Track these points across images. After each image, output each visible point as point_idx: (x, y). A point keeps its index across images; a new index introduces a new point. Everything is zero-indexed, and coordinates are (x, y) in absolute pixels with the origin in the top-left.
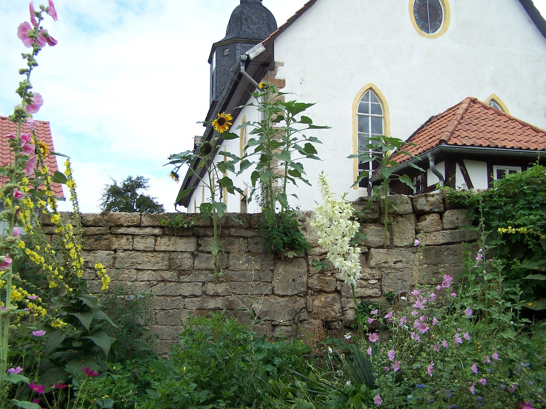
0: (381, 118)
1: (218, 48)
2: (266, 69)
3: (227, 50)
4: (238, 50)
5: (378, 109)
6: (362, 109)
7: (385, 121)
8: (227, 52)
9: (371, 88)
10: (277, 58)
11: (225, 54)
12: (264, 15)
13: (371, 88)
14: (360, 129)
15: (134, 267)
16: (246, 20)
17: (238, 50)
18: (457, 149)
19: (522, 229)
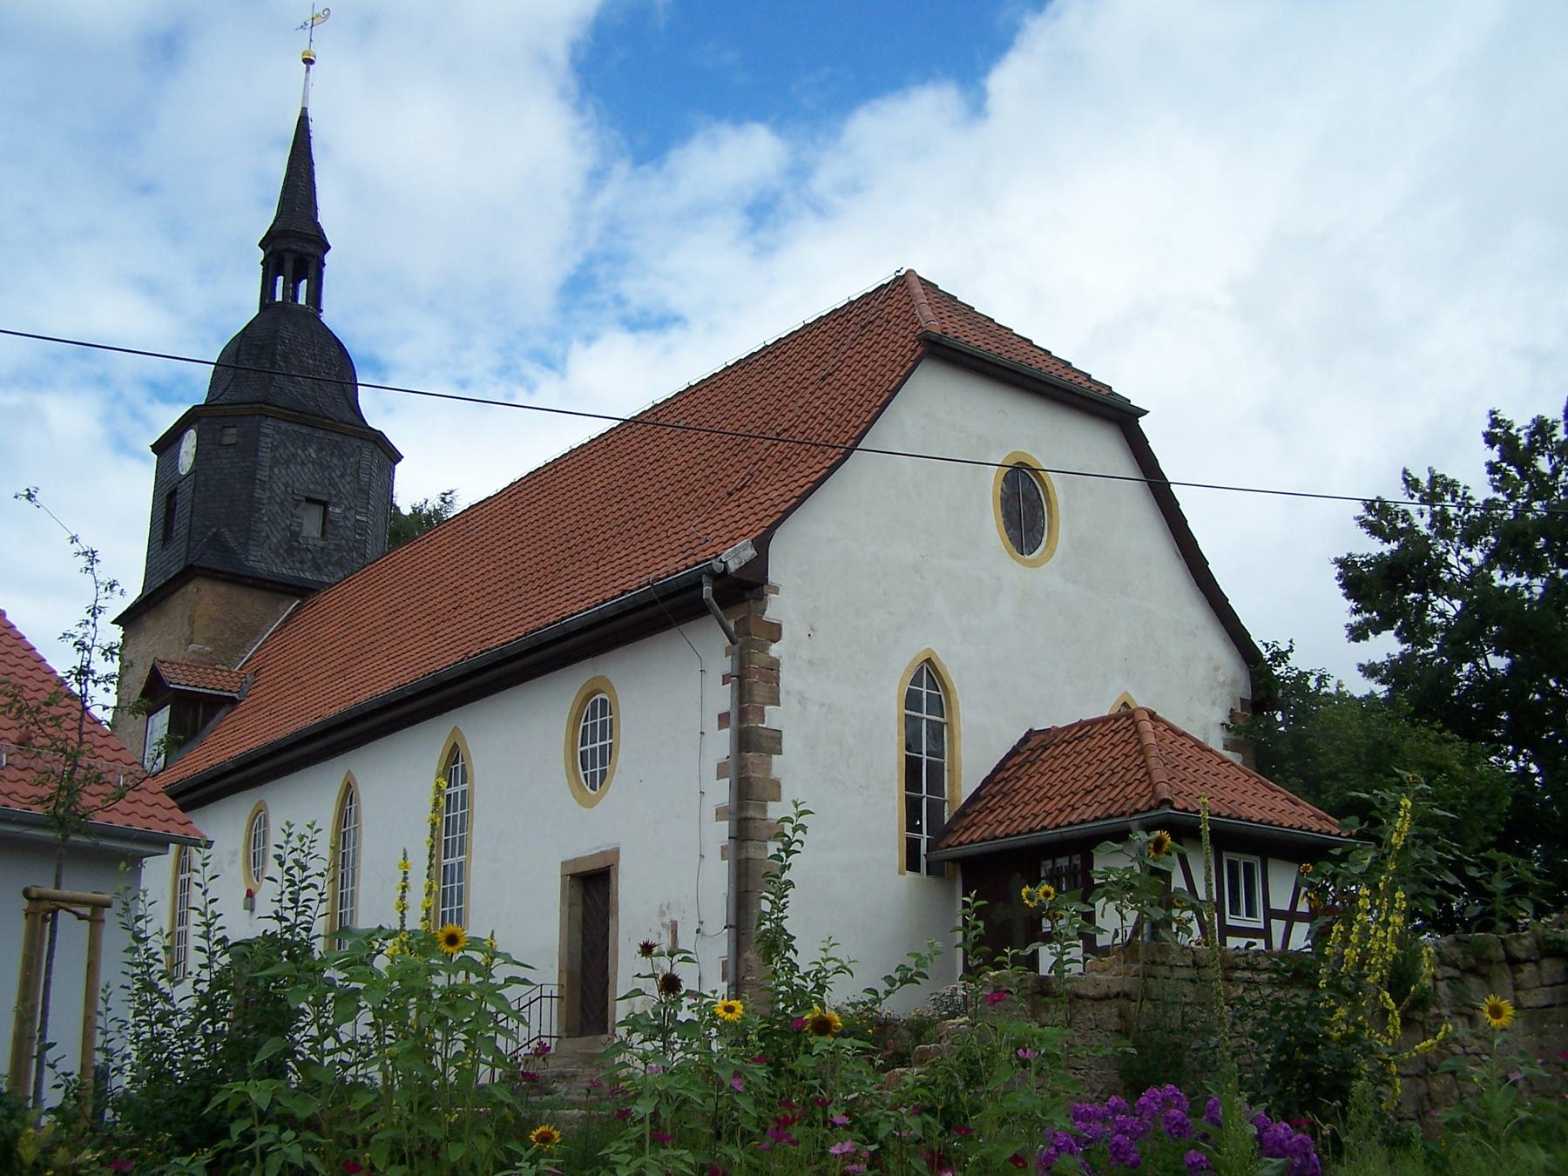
0: (942, 725)
1: (204, 420)
2: (747, 595)
3: (233, 431)
4: (266, 435)
5: (938, 705)
6: (912, 700)
7: (951, 731)
8: (230, 437)
9: (928, 661)
10: (772, 578)
11: (227, 440)
12: (333, 352)
13: (928, 661)
14: (908, 748)
15: (706, 1000)
16: (285, 358)
17: (266, 435)
18: (1020, 841)
19: (1451, 882)
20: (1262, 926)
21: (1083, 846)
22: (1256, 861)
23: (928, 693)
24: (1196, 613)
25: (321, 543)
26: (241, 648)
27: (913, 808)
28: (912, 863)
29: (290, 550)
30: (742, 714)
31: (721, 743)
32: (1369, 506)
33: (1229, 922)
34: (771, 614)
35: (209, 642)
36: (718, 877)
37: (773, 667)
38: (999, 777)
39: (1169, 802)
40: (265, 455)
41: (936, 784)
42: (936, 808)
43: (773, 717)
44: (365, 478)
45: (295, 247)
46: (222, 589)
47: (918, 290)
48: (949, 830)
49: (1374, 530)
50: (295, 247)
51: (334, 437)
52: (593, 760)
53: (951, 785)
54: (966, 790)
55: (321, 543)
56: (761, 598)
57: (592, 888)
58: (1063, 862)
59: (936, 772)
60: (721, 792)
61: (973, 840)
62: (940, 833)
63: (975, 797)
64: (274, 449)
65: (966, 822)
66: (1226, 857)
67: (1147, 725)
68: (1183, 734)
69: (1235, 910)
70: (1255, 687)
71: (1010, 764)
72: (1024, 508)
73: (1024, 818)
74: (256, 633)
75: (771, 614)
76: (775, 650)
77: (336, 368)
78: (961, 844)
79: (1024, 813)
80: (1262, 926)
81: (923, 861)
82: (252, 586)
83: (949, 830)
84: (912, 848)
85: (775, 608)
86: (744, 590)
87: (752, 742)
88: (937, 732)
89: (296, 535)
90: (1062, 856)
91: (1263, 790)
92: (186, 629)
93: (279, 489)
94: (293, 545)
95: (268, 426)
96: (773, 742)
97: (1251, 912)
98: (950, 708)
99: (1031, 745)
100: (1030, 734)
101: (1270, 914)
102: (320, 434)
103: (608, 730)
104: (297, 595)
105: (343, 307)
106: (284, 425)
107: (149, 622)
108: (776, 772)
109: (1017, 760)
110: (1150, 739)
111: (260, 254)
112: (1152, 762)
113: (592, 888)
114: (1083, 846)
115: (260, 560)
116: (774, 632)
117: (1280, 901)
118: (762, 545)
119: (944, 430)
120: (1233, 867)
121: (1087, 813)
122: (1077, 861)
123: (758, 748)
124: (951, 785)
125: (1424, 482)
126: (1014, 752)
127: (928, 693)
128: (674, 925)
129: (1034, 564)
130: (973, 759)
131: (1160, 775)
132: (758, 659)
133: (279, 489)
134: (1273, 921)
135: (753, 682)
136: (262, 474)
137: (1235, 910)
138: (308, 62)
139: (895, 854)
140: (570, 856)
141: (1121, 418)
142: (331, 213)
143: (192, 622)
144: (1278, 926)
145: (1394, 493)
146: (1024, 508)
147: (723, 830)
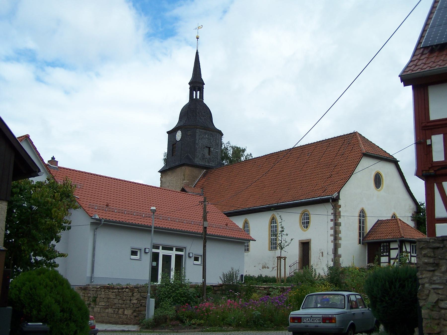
5: (364, 216)
6: (360, 216)
21: (389, 242)
23: (362, 214)
24: (407, 196)
25: (209, 157)
26: (194, 181)
27: (360, 233)
28: (360, 243)
29: (203, 159)
30: (335, 220)
31: (332, 224)
34: (339, 204)
35: (188, 180)
36: (331, 246)
37: (340, 212)
39: (403, 237)
40: (197, 137)
41: (363, 230)
42: (363, 233)
43: (340, 220)
44: (217, 141)
45: (197, 84)
46: (190, 168)
47: (358, 135)
48: (365, 237)
50: (197, 84)
51: (211, 132)
52: (306, 223)
54: (368, 230)
55: (209, 157)
56: (338, 201)
57: (305, 246)
58: (385, 244)
60: (332, 232)
61: (371, 239)
62: (364, 238)
64: (199, 136)
66: (412, 244)
67: (399, 222)
70: (417, 210)
72: (378, 181)
74: (197, 177)
75: (339, 204)
76: (340, 209)
77: (207, 113)
82: (196, 167)
84: (360, 240)
85: (341, 202)
86: (336, 200)
87: (337, 224)
89: (204, 155)
91: (418, 233)
92: (183, 177)
93: (200, 145)
94: (203, 158)
95: (198, 131)
96: (340, 224)
102: (208, 132)
103: (308, 218)
104: (205, 169)
105: (209, 99)
106: (201, 130)
107: (169, 173)
108: (340, 229)
110: (400, 225)
111: (189, 86)
112: (400, 229)
113: (305, 246)
114: (389, 242)
115: (197, 161)
116: (340, 206)
118: (339, 193)
119: (366, 169)
120: (413, 246)
121: (390, 237)
123: (338, 225)
126: (376, 224)
127: (362, 214)
128: (322, 253)
129: (379, 190)
130: (370, 224)
131: (402, 232)
132: (338, 211)
133: (200, 145)
135: (336, 215)
136: (197, 142)
137: (413, 253)
138: (198, 38)
139: (357, 241)
140: (301, 239)
141: (395, 162)
142: (205, 76)
143: (184, 175)
146: (378, 181)
147: (332, 238)
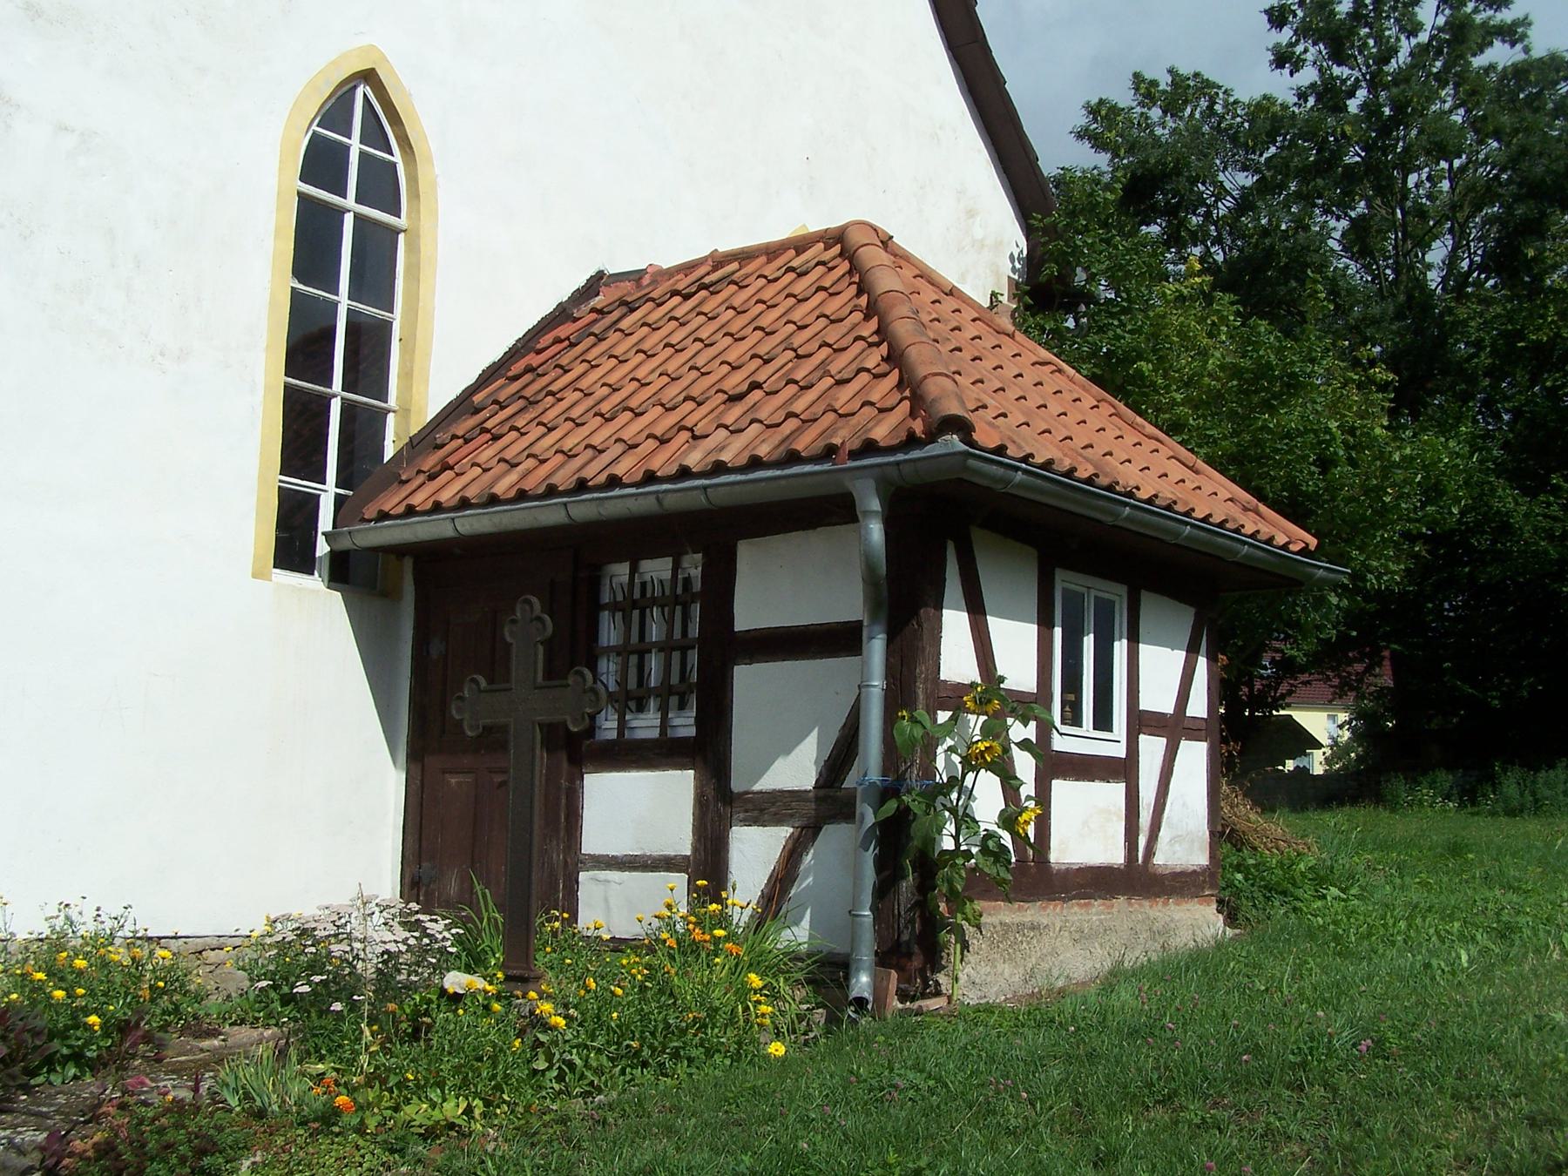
5: (382, 186)
6: (322, 163)
7: (413, 249)
13: (369, 76)
20: (1120, 751)
22: (1117, 594)
28: (292, 549)
32: (1093, 111)
33: (1059, 744)
38: (517, 368)
39: (961, 426)
42: (363, 428)
49: (1098, 143)
53: (407, 375)
58: (657, 569)
59: (370, 346)
61: (430, 509)
63: (463, 405)
65: (431, 461)
67: (872, 256)
68: (952, 292)
69: (1073, 715)
71: (547, 339)
73: (570, 456)
78: (411, 511)
79: (568, 444)
80: (1120, 751)
81: (322, 548)
83: (392, 477)
88: (377, 250)
90: (654, 554)
97: (1103, 720)
98: (415, 194)
99: (598, 301)
100: (597, 282)
101: (1141, 722)
109: (564, 330)
114: (714, 528)
117: (1158, 697)
122: (693, 566)
124: (407, 375)
125: (1165, 81)
126: (561, 314)
134: (1144, 739)
139: (251, 522)
144: (1152, 748)
145: (1124, 97)
